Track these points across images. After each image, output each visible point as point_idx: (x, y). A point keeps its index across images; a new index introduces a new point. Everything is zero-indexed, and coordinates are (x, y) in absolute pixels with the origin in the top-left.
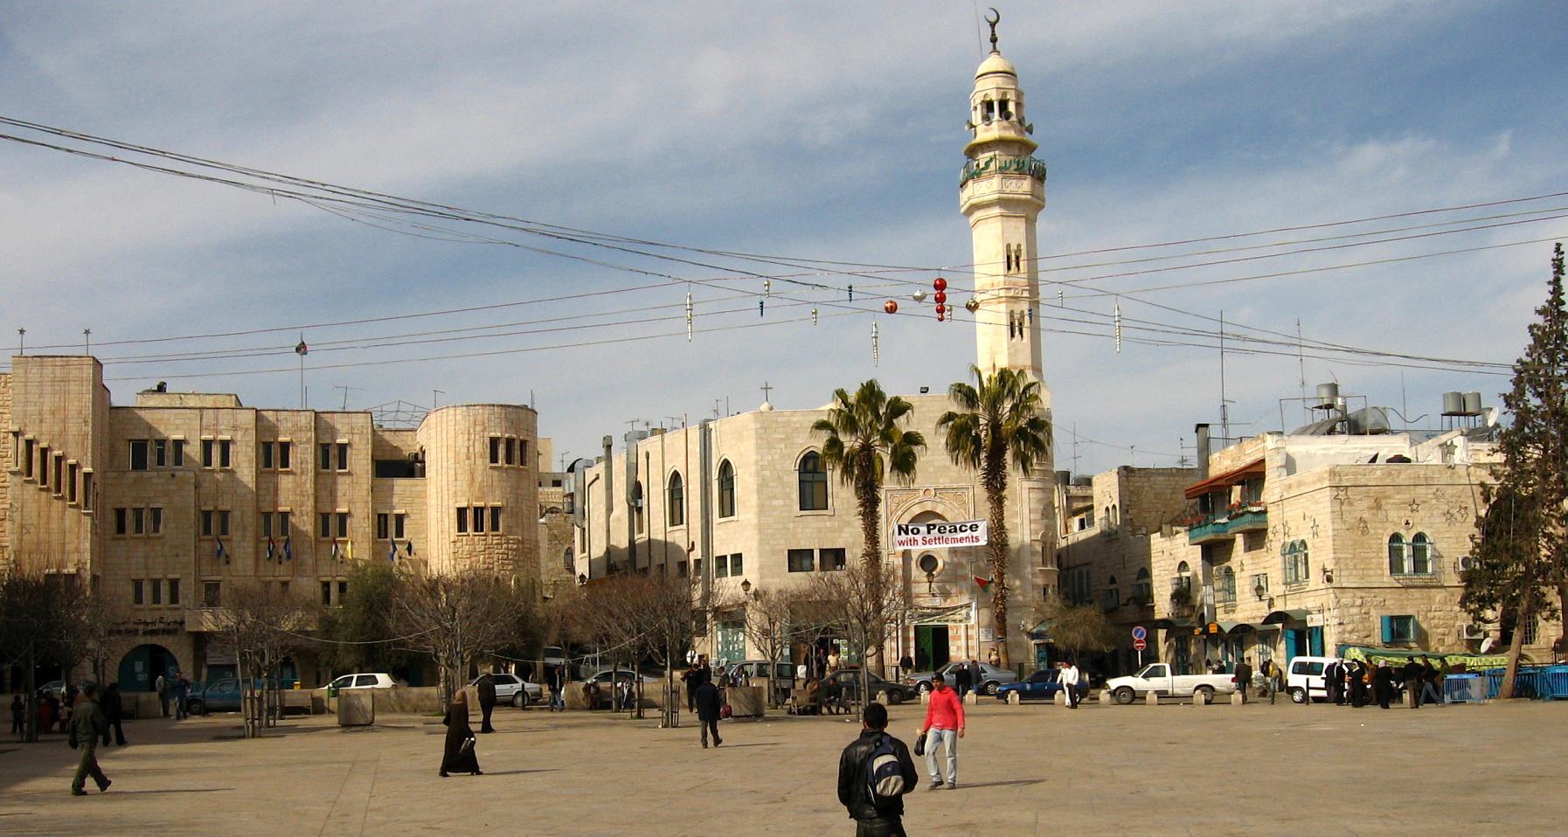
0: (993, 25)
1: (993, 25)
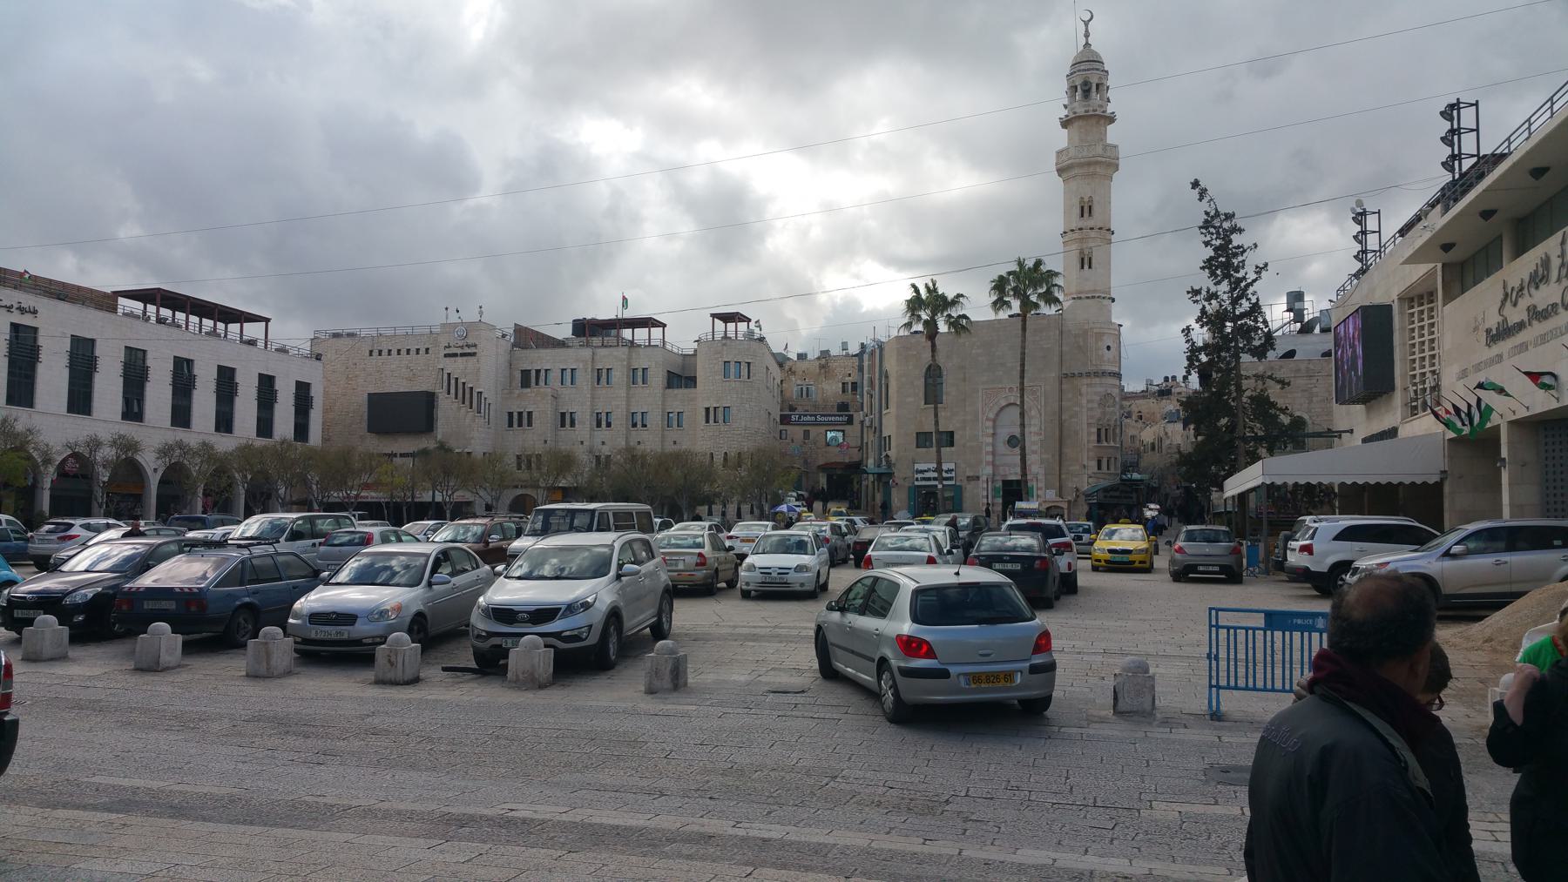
0: (1086, 24)
1: (1086, 24)
